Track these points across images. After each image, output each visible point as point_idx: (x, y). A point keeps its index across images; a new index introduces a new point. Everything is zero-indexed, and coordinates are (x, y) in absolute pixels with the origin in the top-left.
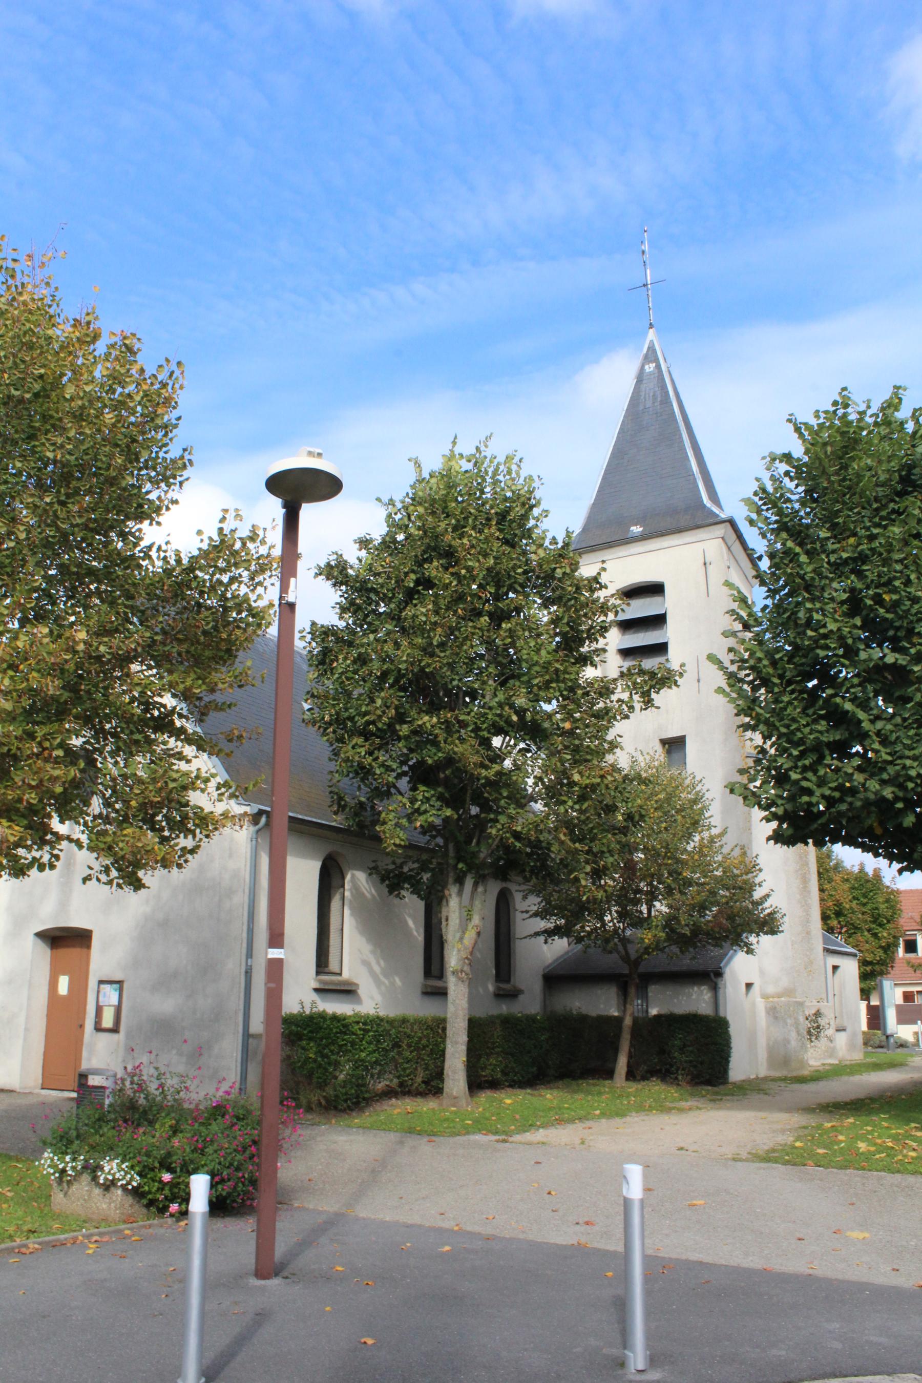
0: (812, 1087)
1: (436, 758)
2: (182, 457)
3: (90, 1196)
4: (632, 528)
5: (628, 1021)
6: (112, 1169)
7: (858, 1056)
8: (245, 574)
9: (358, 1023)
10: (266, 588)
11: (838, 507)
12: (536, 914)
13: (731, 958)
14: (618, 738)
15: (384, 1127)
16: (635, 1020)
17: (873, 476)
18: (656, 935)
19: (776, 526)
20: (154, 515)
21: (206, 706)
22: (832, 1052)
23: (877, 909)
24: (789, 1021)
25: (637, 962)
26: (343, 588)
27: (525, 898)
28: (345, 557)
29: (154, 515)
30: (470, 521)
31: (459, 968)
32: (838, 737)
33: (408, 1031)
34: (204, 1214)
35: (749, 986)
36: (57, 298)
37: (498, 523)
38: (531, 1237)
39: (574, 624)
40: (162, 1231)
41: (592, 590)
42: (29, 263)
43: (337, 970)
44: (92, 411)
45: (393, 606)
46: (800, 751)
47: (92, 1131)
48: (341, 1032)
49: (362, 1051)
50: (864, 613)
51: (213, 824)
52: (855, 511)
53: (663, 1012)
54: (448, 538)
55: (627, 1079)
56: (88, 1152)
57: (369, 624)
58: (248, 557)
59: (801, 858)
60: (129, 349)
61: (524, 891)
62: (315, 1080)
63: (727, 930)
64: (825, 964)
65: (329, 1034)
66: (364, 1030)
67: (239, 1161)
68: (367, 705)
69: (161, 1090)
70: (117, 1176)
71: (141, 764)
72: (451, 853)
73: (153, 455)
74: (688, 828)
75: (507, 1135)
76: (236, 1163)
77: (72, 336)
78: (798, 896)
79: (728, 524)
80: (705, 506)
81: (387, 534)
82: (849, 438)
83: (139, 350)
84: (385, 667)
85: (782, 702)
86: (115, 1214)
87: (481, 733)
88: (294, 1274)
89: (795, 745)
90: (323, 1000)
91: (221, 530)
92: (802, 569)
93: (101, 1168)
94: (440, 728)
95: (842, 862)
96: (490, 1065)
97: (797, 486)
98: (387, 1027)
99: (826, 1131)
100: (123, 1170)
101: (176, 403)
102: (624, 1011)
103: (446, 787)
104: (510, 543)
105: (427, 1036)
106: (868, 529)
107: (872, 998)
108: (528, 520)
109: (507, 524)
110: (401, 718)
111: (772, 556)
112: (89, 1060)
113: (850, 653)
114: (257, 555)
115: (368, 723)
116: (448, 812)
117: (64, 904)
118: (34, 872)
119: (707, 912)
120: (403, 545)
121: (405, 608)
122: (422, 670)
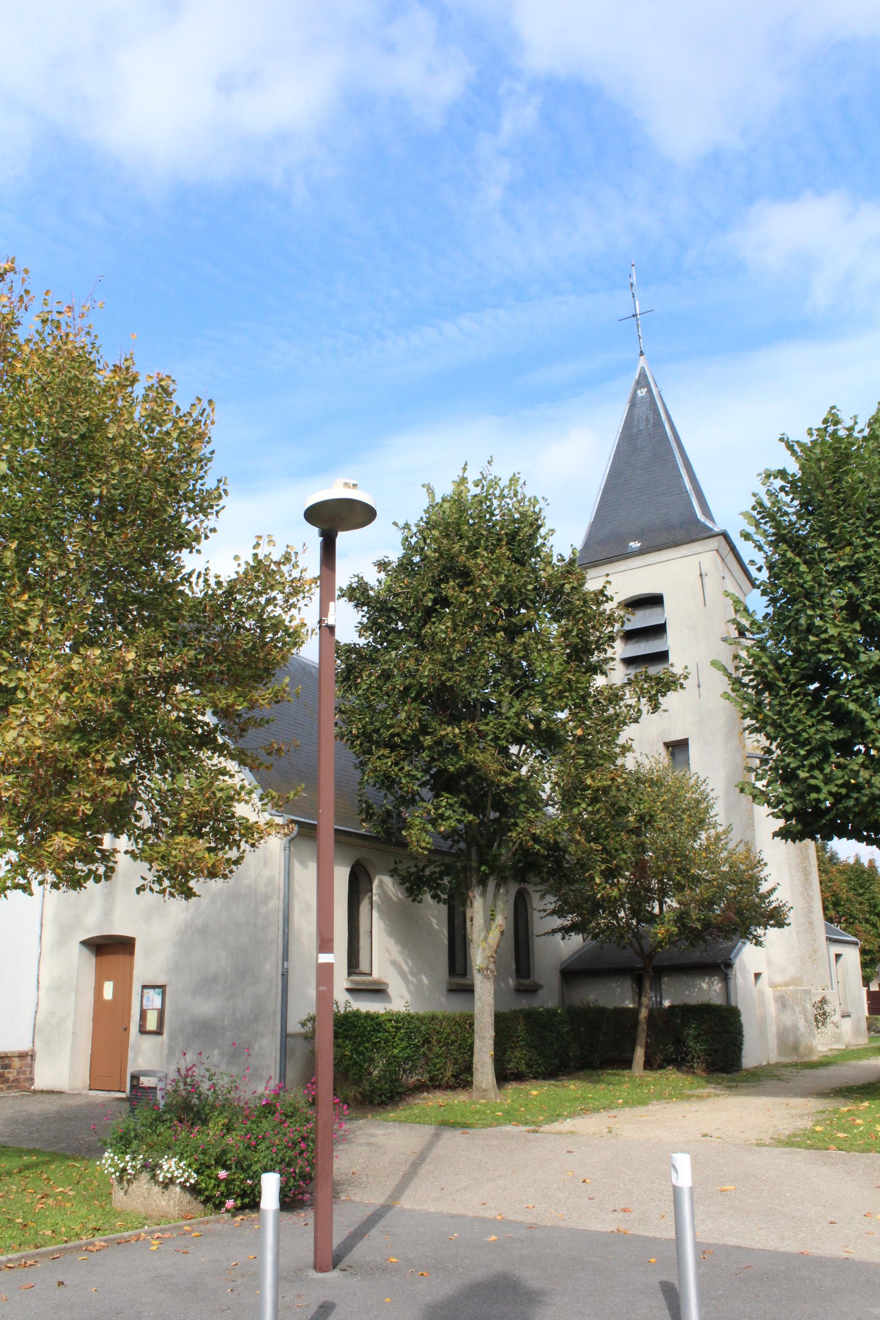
0: (822, 1072)
1: (458, 766)
2: (218, 488)
3: (149, 1194)
4: (631, 544)
5: (644, 1013)
6: (170, 1167)
7: (863, 1040)
8: (280, 597)
9: (390, 1021)
10: (299, 609)
11: (834, 518)
12: (553, 913)
13: (740, 950)
14: (630, 742)
15: (419, 1120)
16: (651, 1012)
17: (865, 488)
18: (668, 930)
19: (773, 538)
20: (194, 544)
21: (245, 723)
22: (838, 1038)
23: (873, 898)
24: (797, 1009)
25: (651, 956)
26: (365, 608)
27: (542, 897)
28: (366, 580)
29: (194, 544)
30: (482, 542)
31: (484, 966)
32: (841, 736)
33: (438, 1027)
34: (275, 1211)
35: (757, 976)
36: (97, 345)
37: (508, 543)
38: (571, 1225)
39: (581, 634)
40: (219, 1226)
41: (599, 603)
42: (70, 314)
43: (368, 971)
44: (133, 449)
45: (412, 624)
46: (806, 751)
47: (149, 1131)
48: (375, 1030)
49: (394, 1048)
50: (863, 617)
51: (258, 833)
52: (851, 521)
53: (677, 1003)
54: (462, 559)
55: (645, 1068)
56: (146, 1151)
57: (390, 642)
58: (282, 580)
59: (801, 851)
60: (165, 390)
61: (541, 891)
62: (351, 1077)
63: (736, 924)
64: (828, 952)
65: (364, 1032)
66: (396, 1027)
67: (290, 1157)
68: (391, 718)
69: (212, 1090)
70: (176, 1174)
71: (186, 782)
72: (474, 857)
73: (191, 488)
74: (694, 827)
75: (536, 1126)
76: (287, 1159)
77: (113, 380)
78: (800, 889)
79: (722, 537)
80: (699, 521)
81: (403, 557)
82: (841, 453)
83: (174, 390)
84: (408, 681)
85: (788, 704)
86: (174, 1211)
87: (500, 743)
88: (351, 1267)
89: (802, 745)
90: (355, 1000)
91: (255, 555)
92: (802, 578)
93: (161, 1167)
94: (461, 738)
95: (837, 854)
96: (516, 1057)
97: (792, 500)
98: (418, 1024)
99: (843, 1115)
100: (182, 1168)
101: (209, 438)
102: (640, 1003)
103: (468, 794)
104: (520, 561)
105: (455, 1032)
106: (862, 538)
107: (871, 984)
108: (537, 540)
109: (516, 544)
110: (424, 730)
111: (771, 567)
112: (135, 1060)
113: (851, 656)
114: (291, 579)
115: (393, 735)
116: (471, 817)
117: (107, 914)
118: (90, 883)
119: (715, 907)
120: (419, 567)
121: (424, 626)
122: (443, 684)
